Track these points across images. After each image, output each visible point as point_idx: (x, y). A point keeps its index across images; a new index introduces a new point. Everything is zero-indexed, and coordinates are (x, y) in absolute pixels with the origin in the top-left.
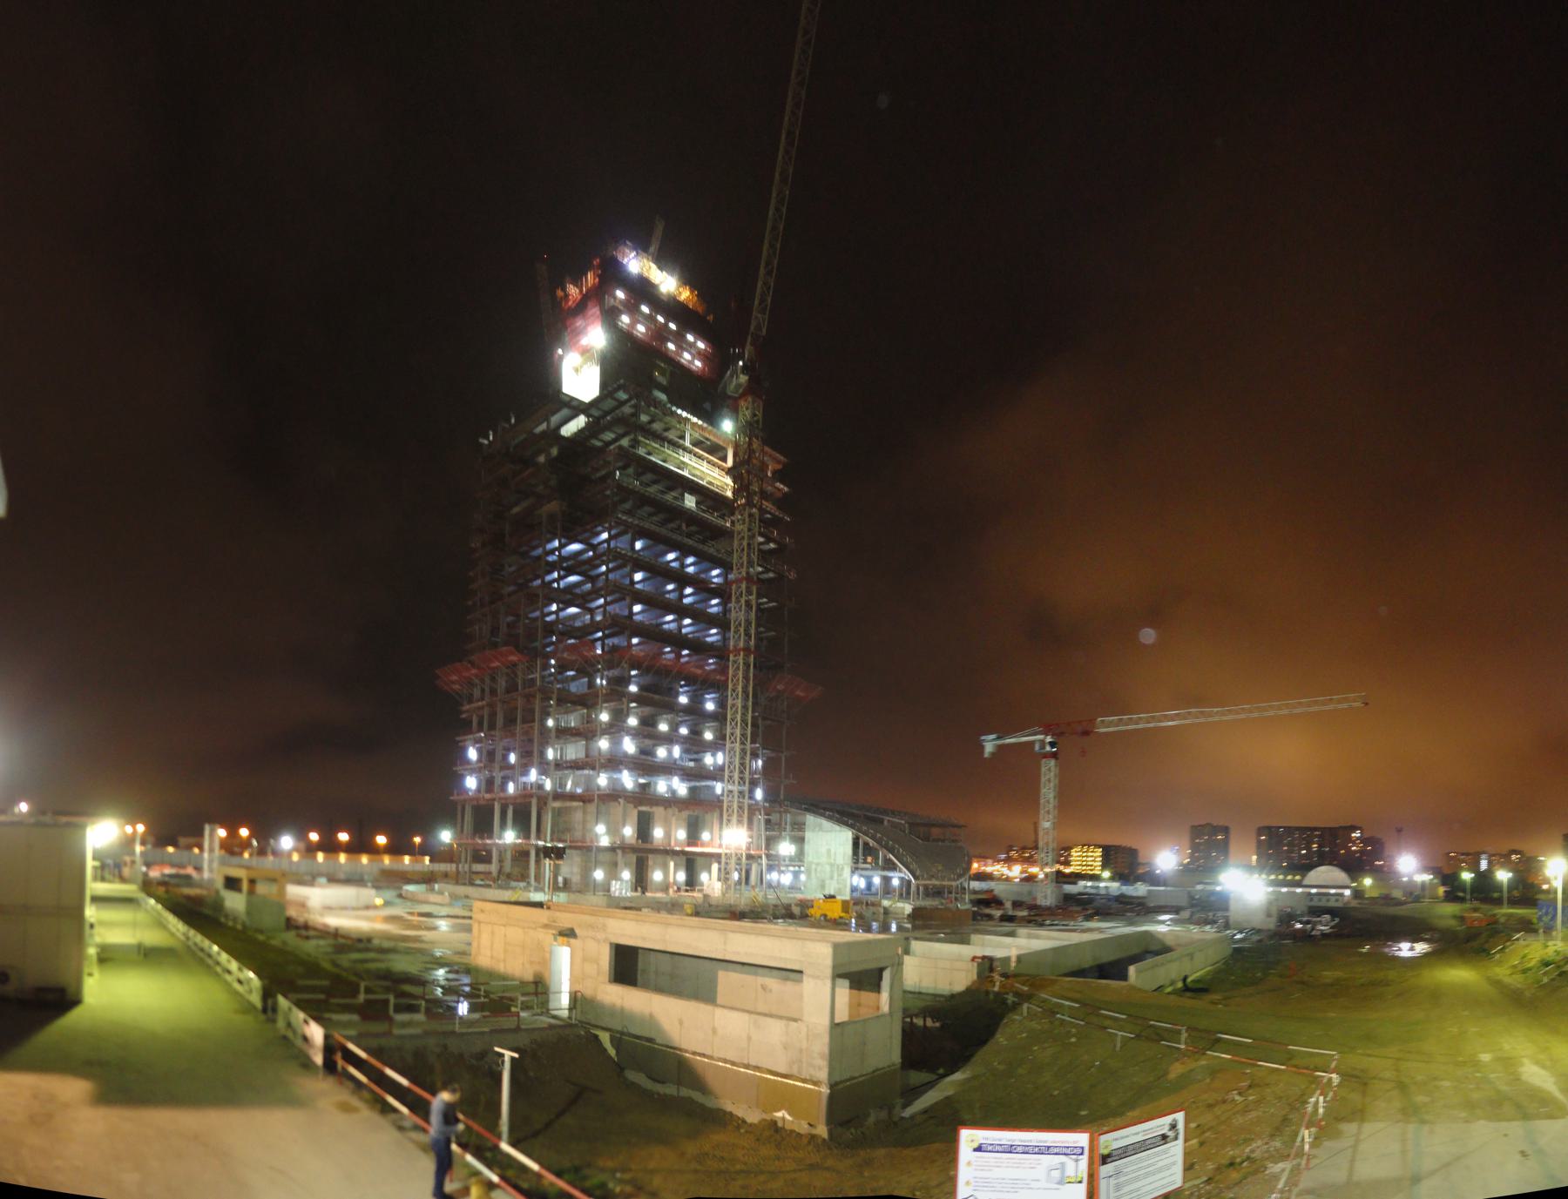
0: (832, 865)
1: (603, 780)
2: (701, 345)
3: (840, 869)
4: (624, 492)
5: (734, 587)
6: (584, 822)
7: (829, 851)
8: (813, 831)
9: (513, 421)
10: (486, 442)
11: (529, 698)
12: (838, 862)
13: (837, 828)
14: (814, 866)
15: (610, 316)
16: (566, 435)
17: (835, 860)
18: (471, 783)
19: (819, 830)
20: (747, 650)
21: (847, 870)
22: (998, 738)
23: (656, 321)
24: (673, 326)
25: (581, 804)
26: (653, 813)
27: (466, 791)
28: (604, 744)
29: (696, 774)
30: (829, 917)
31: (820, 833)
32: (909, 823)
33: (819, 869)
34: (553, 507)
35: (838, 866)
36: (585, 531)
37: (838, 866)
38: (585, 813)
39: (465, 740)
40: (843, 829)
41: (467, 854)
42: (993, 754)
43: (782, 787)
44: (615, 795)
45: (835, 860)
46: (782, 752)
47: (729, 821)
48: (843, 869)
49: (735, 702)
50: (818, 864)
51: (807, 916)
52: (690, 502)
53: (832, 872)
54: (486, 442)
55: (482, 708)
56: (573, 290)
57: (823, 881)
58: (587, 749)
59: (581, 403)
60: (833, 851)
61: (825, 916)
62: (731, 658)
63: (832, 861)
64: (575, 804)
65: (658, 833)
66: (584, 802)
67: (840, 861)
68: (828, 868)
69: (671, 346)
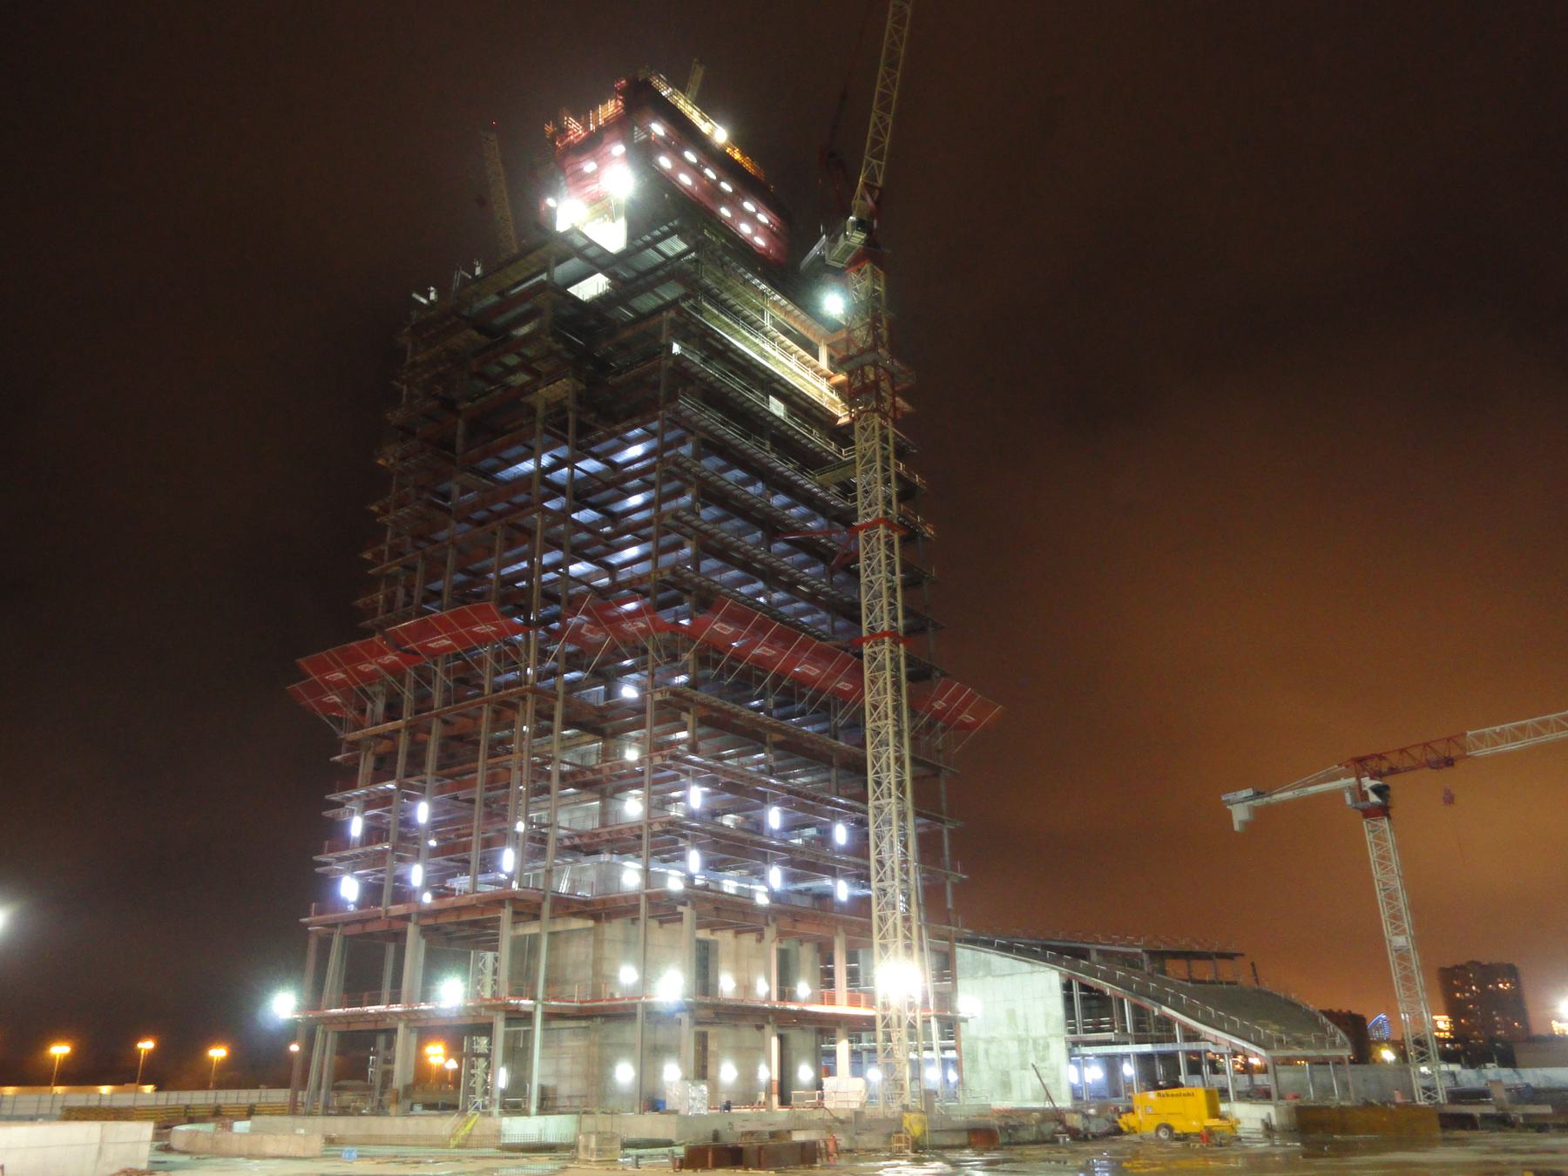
0: (1021, 1041)
1: (631, 876)
2: (763, 218)
3: (1042, 1047)
4: (680, 370)
5: (861, 534)
6: (597, 963)
7: (1012, 1014)
8: (974, 976)
9: (478, 271)
10: (424, 301)
11: (504, 712)
12: (1033, 1034)
13: (1025, 967)
14: (981, 1046)
15: (644, 153)
16: (581, 298)
17: (1027, 1030)
18: (349, 889)
19: (985, 976)
20: (892, 634)
21: (1058, 1049)
22: (1258, 794)
23: (703, 175)
24: (726, 187)
25: (591, 923)
26: (716, 942)
27: (340, 904)
28: (633, 807)
29: (807, 863)
30: (1177, 1131)
31: (990, 979)
32: (1146, 952)
33: (994, 1050)
34: (561, 389)
35: (1035, 1042)
36: (610, 436)
37: (1035, 1042)
38: (599, 943)
39: (340, 805)
40: (1037, 968)
41: (324, 1053)
42: (1245, 824)
43: (949, 889)
44: (663, 908)
45: (1027, 1030)
46: (943, 822)
47: (884, 947)
48: (1047, 1047)
49: (879, 723)
50: (990, 1041)
51: (1119, 1131)
52: (777, 408)
53: (1023, 1054)
54: (424, 301)
55: (392, 736)
56: (575, 129)
57: (1006, 1074)
58: (604, 813)
59: (604, 252)
60: (1020, 1012)
61: (1169, 1128)
62: (866, 650)
63: (1021, 1032)
64: (576, 924)
65: (727, 985)
66: (596, 917)
67: (1038, 1030)
68: (1013, 1047)
69: (725, 212)
